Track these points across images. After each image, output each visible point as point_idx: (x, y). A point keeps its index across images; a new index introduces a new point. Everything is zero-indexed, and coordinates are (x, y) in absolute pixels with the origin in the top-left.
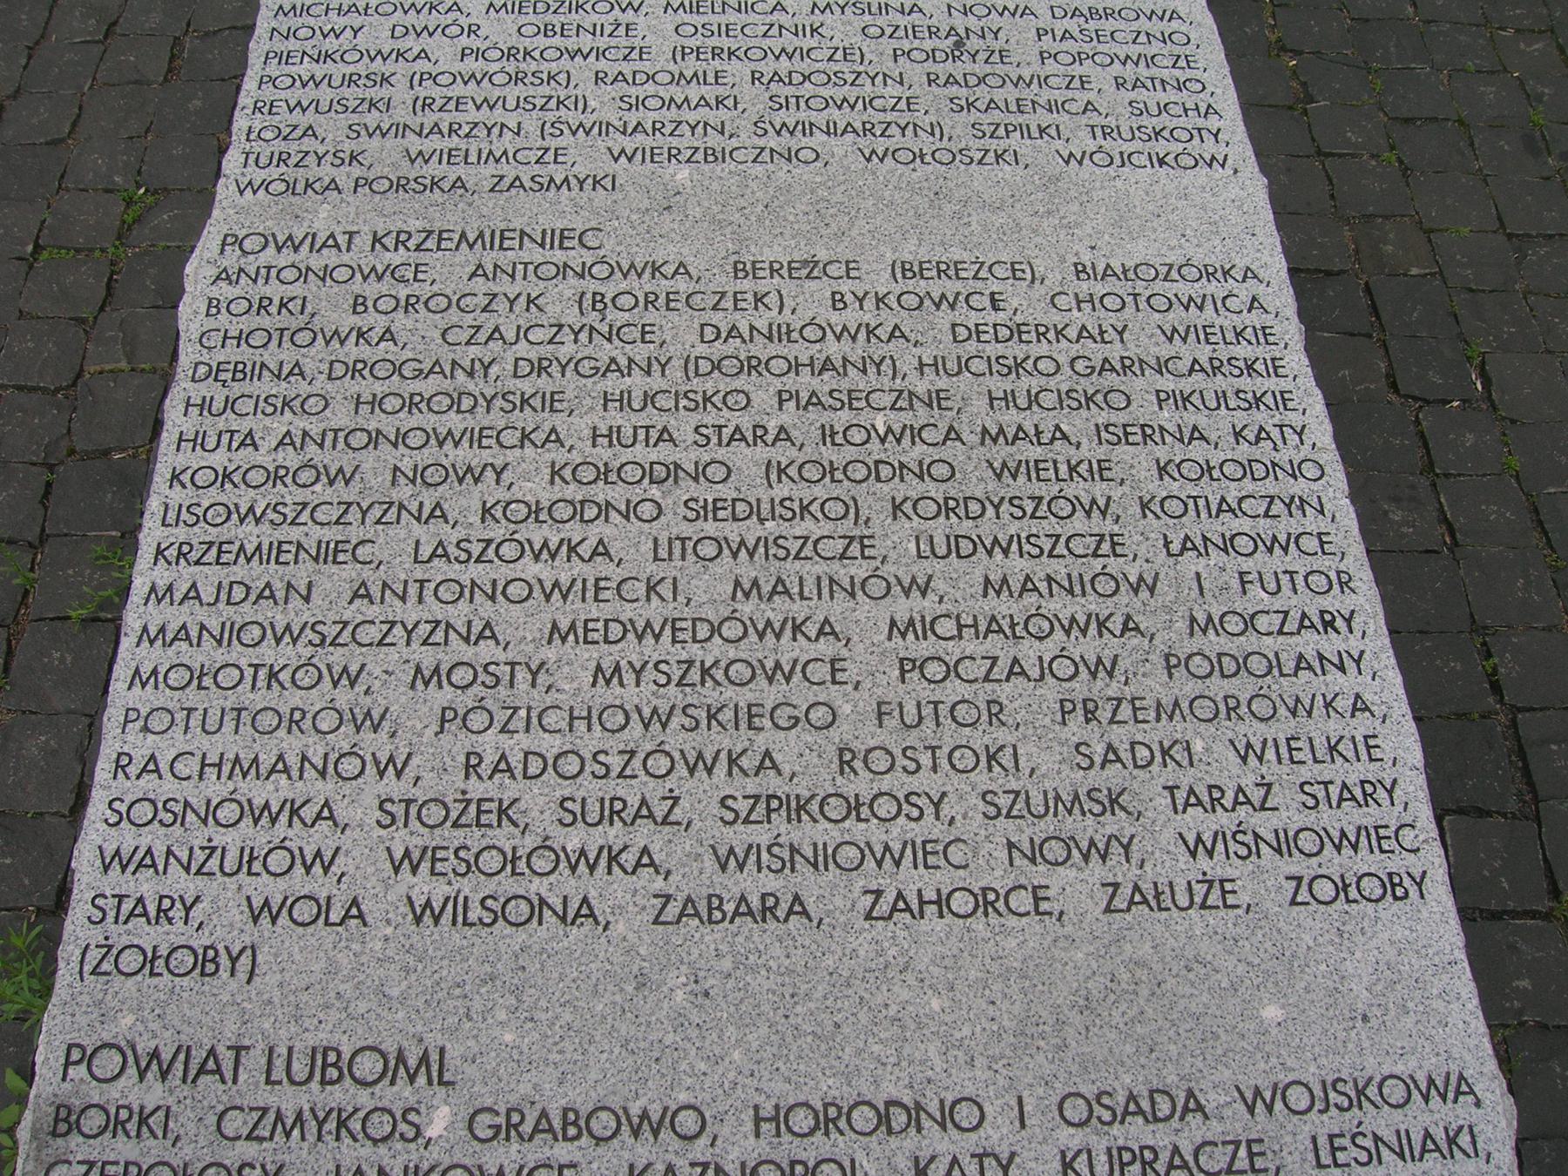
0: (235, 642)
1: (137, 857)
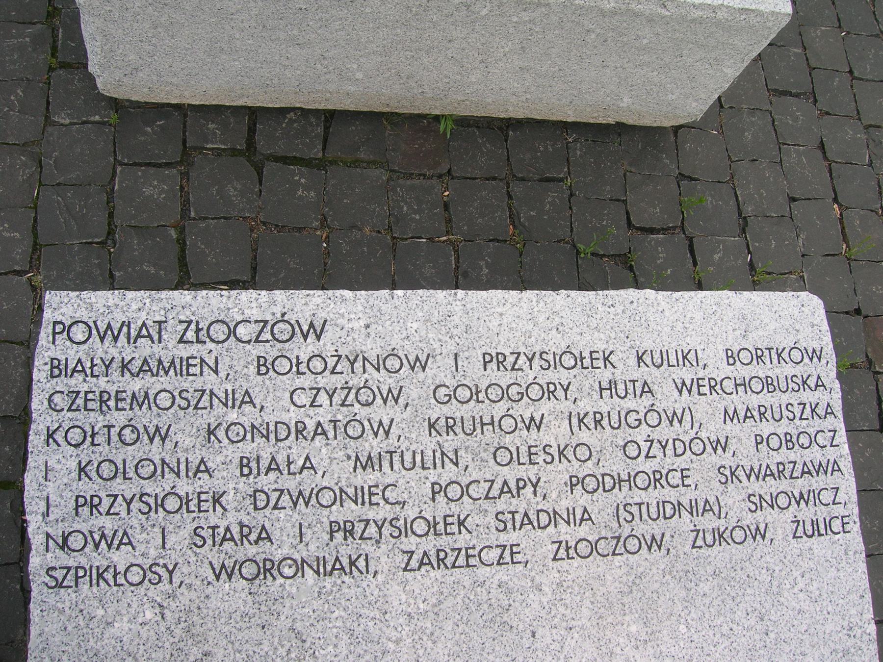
1: (763, 472)
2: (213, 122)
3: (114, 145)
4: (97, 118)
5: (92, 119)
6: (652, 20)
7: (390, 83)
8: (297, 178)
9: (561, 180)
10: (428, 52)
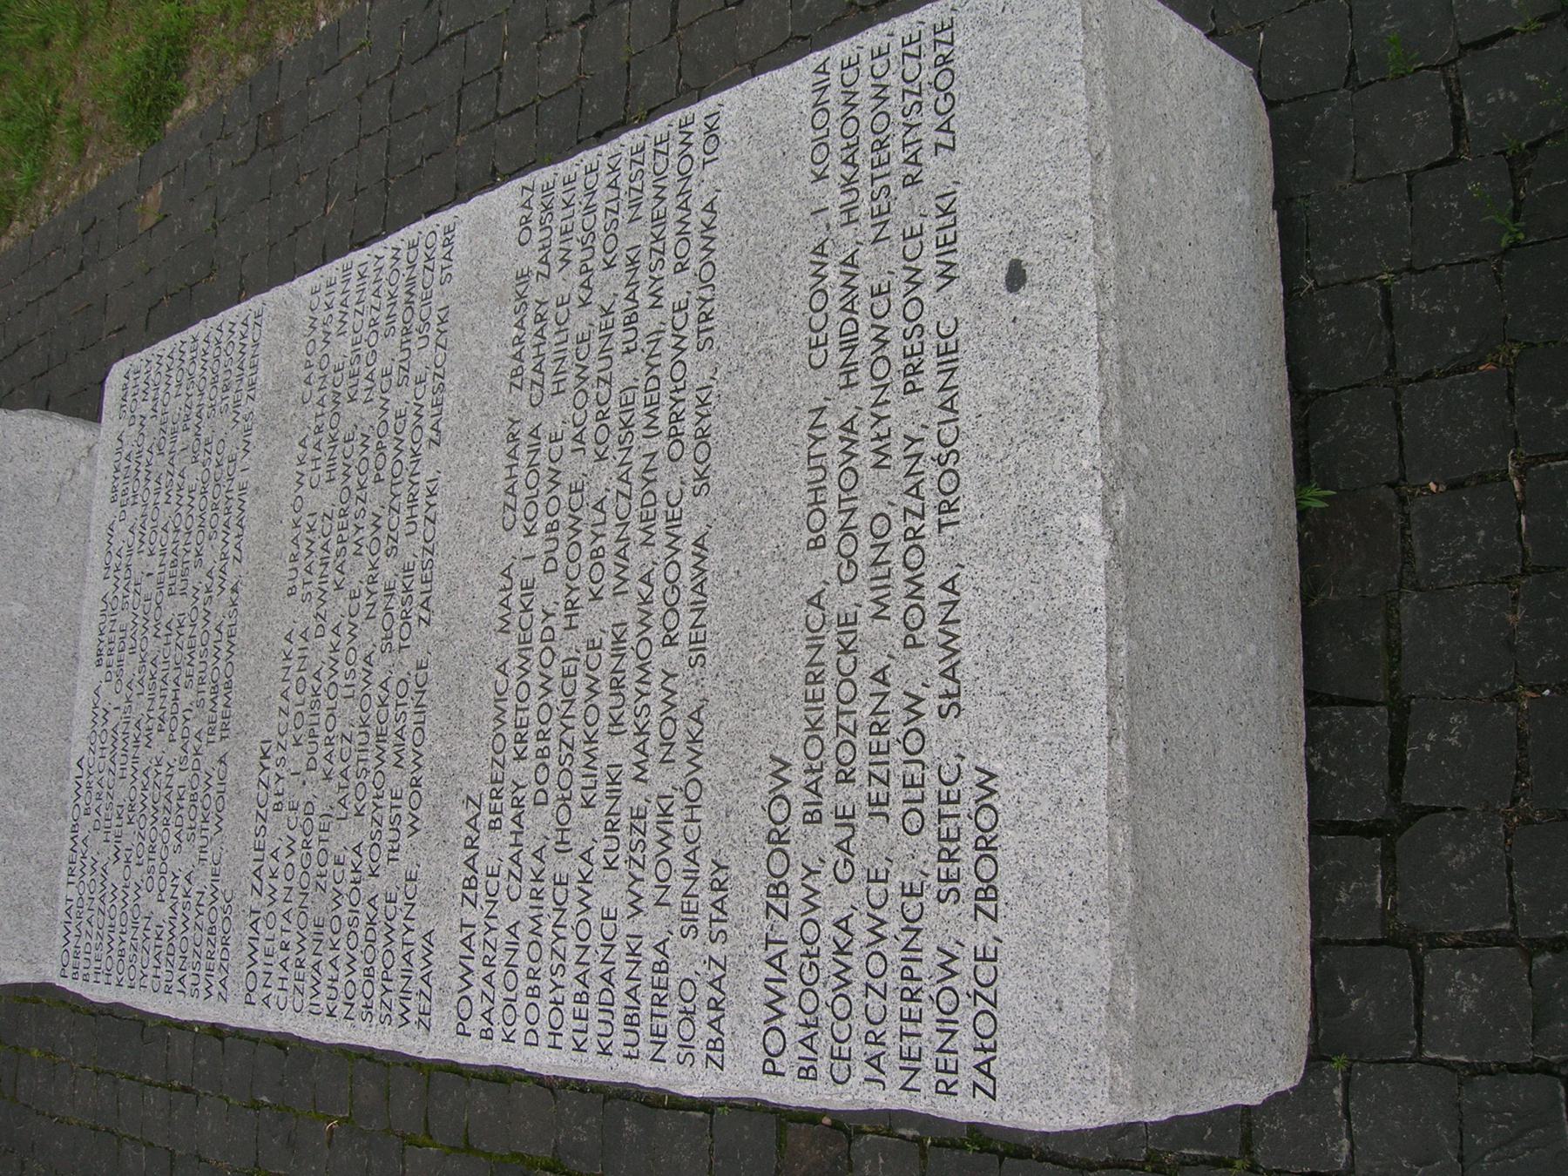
0: (953, 1017)
2: (1337, 895)
3: (1384, 1062)
4: (1338, 1092)
5: (1339, 1100)
6: (1121, 172)
7: (1257, 596)
8: (1428, 747)
9: (1386, 290)
10: (1209, 538)
